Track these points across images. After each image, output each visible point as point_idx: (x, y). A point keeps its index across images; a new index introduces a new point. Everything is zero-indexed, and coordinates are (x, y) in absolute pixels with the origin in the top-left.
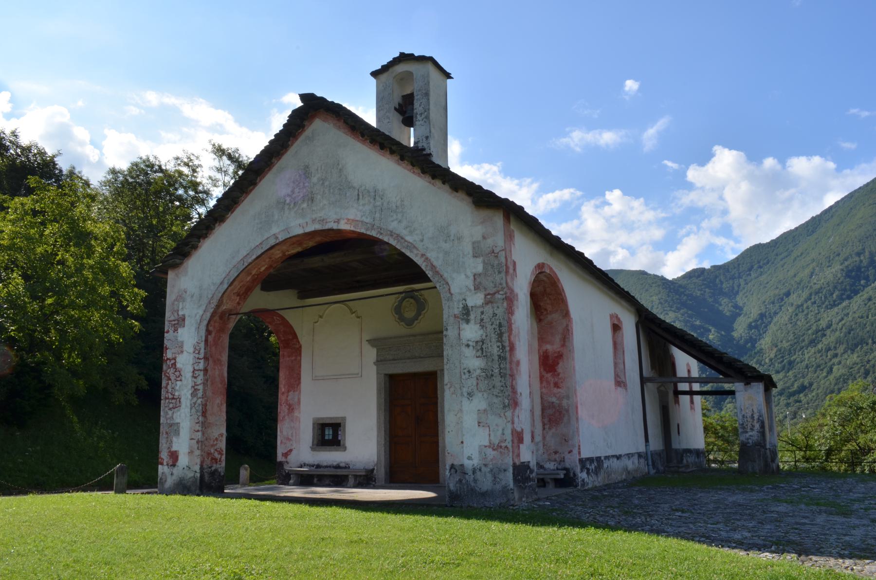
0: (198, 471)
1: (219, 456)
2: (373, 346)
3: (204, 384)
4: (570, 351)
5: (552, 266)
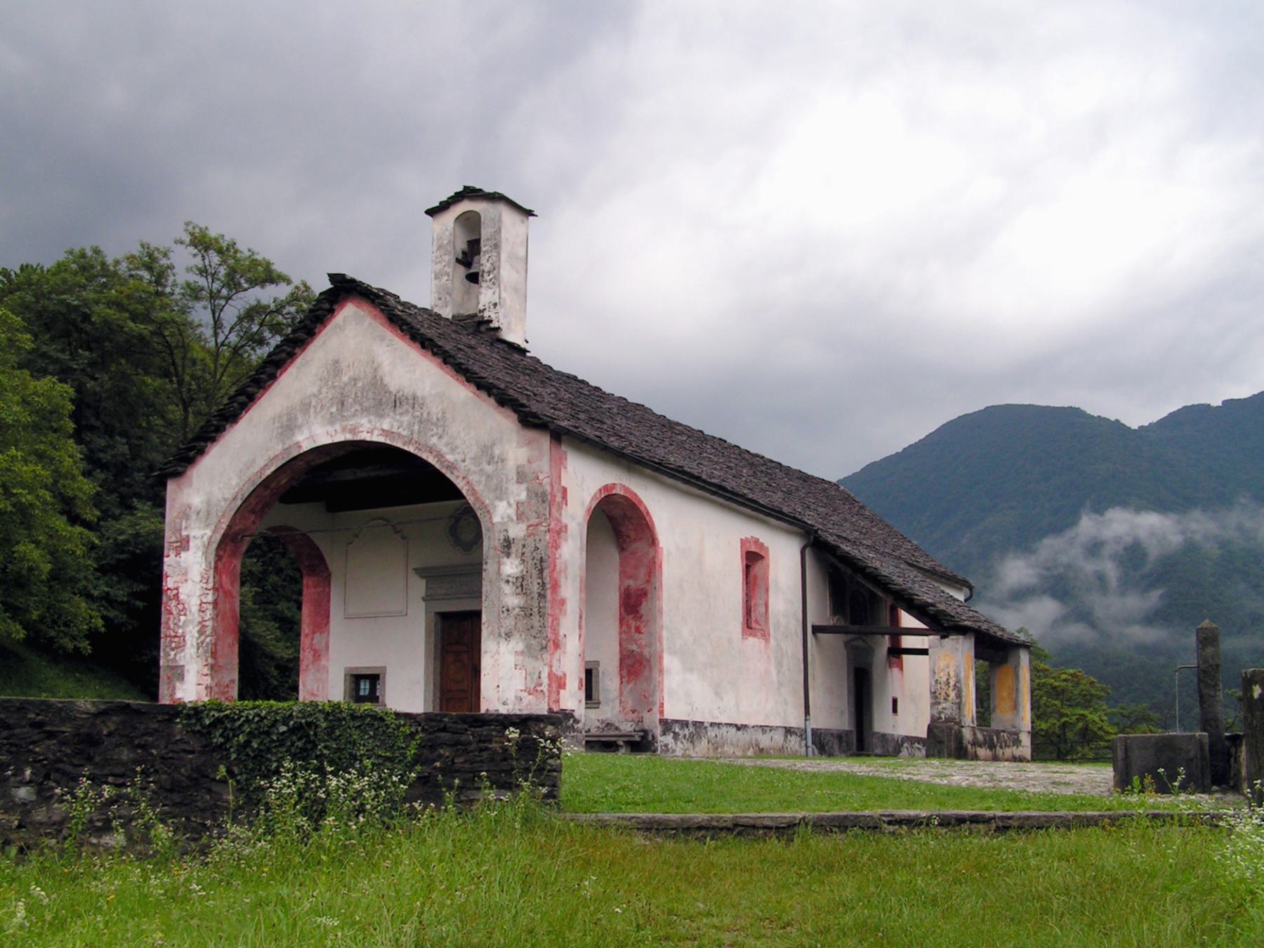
2: (422, 577)
3: (214, 619)
4: (655, 588)
5: (627, 485)
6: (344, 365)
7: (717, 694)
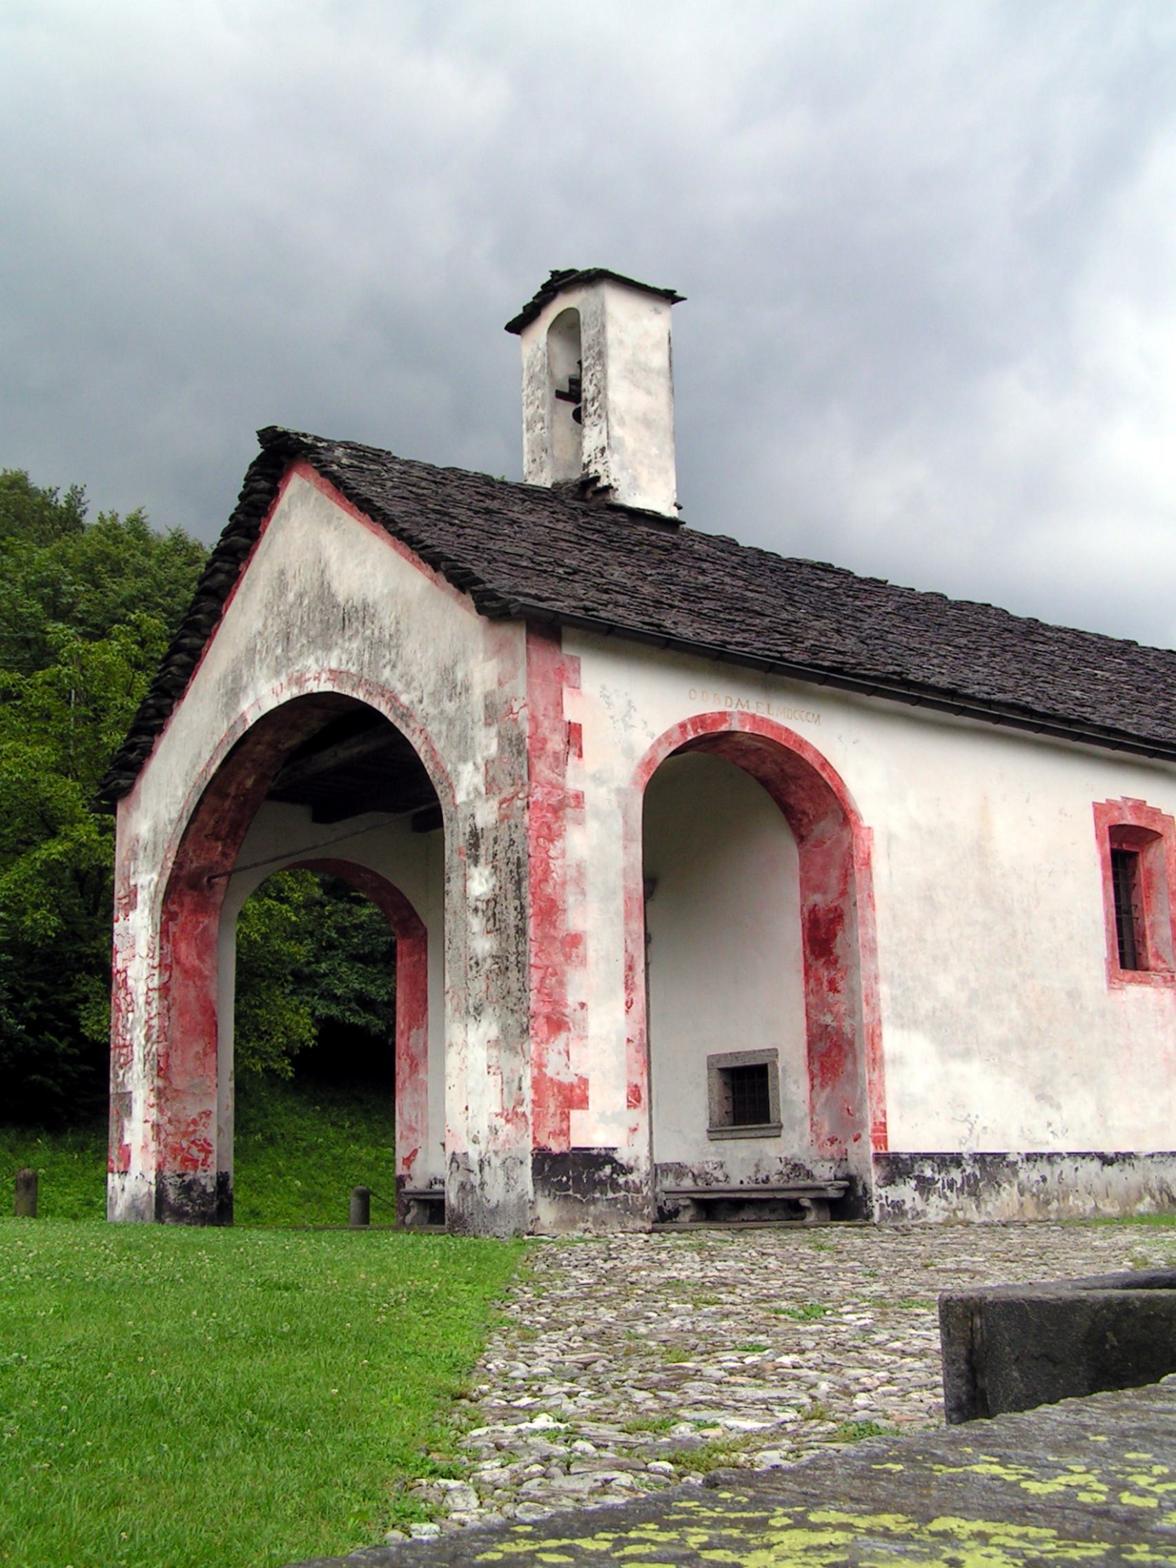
0: (153, 1181)
1: (202, 1155)
4: (855, 904)
6: (290, 574)
7: (1040, 1097)
